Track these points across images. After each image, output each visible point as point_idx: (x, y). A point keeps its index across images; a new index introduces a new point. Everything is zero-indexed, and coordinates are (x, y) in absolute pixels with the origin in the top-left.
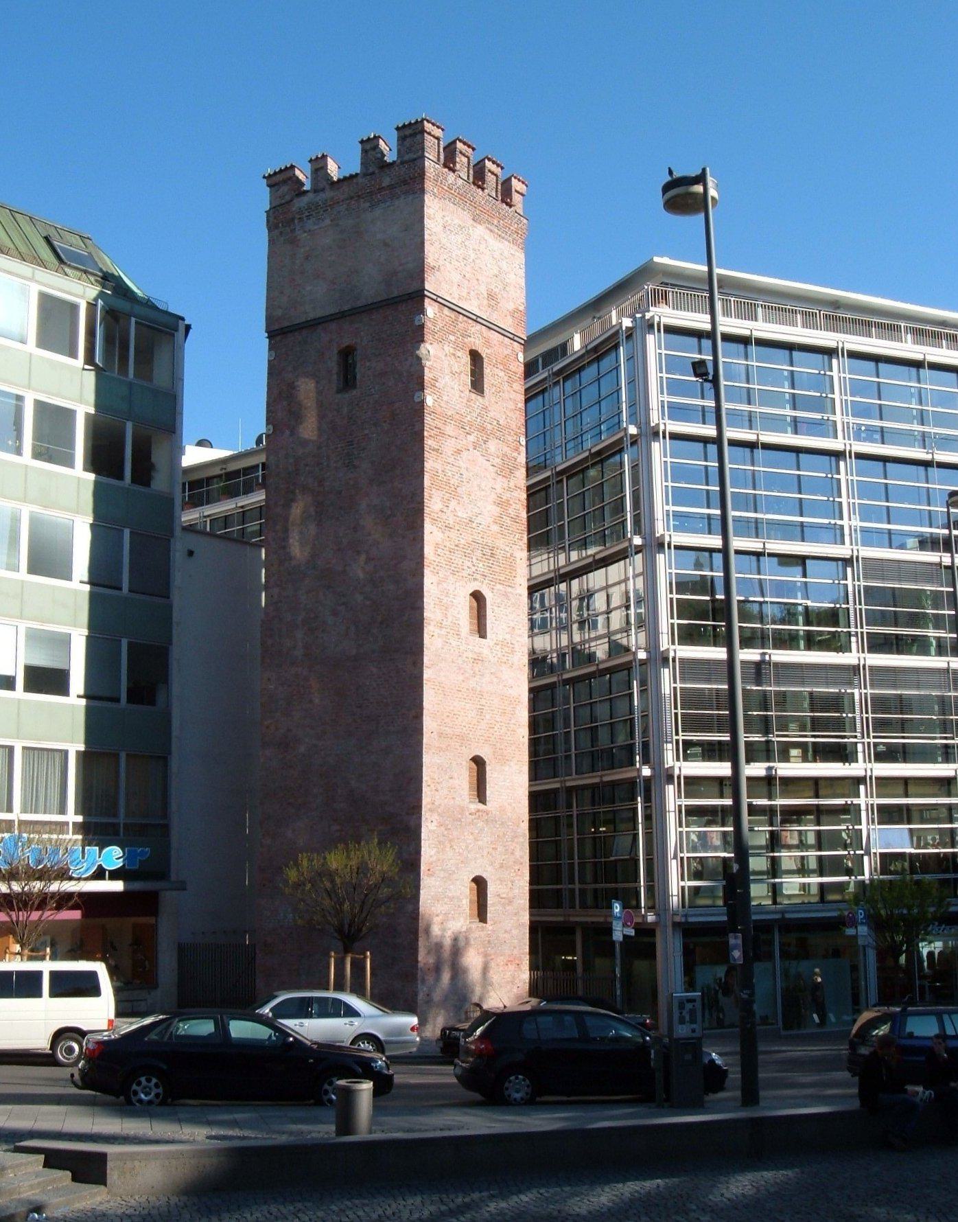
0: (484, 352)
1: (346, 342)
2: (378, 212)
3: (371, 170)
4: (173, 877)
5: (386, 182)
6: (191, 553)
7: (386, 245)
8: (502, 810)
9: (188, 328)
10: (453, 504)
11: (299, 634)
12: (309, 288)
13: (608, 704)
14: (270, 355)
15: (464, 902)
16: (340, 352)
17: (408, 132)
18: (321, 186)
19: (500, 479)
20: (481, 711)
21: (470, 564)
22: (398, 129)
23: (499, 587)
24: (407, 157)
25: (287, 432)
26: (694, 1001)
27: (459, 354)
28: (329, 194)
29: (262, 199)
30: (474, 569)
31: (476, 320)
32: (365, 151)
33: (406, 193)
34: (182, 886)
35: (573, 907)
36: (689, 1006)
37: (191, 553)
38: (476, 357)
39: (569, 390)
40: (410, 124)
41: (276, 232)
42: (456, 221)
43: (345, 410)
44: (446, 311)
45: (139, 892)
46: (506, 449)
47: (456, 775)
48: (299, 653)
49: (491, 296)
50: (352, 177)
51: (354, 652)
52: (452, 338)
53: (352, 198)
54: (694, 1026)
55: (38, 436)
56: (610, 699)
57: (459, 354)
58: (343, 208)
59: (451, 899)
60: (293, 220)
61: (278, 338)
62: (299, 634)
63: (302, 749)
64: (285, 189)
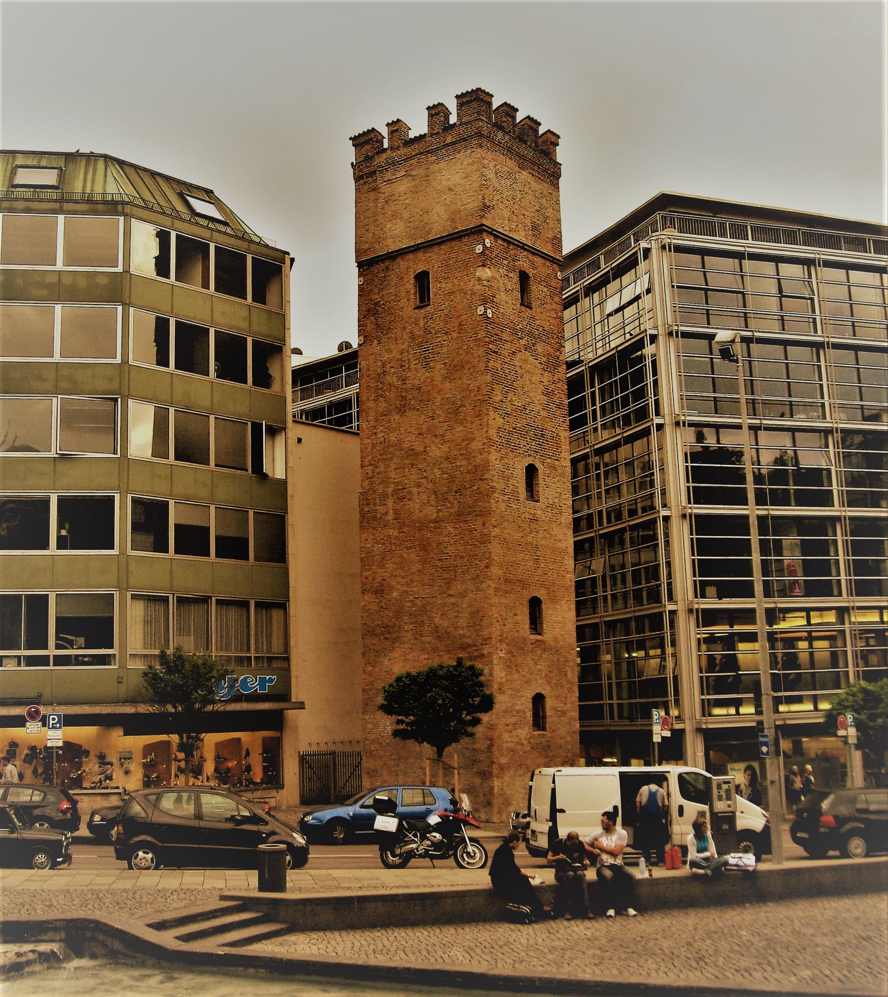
0: (531, 272)
2: (442, 165)
4: (293, 700)
5: (449, 140)
6: (300, 440)
7: (450, 189)
9: (292, 260)
11: (390, 502)
16: (415, 277)
23: (549, 460)
25: (376, 342)
29: (350, 154)
31: (523, 247)
32: (431, 116)
34: (301, 706)
36: (725, 787)
38: (524, 278)
43: (422, 323)
46: (550, 349)
47: (518, 612)
48: (390, 517)
49: (535, 227)
51: (435, 515)
59: (518, 712)
62: (390, 502)
63: (395, 594)
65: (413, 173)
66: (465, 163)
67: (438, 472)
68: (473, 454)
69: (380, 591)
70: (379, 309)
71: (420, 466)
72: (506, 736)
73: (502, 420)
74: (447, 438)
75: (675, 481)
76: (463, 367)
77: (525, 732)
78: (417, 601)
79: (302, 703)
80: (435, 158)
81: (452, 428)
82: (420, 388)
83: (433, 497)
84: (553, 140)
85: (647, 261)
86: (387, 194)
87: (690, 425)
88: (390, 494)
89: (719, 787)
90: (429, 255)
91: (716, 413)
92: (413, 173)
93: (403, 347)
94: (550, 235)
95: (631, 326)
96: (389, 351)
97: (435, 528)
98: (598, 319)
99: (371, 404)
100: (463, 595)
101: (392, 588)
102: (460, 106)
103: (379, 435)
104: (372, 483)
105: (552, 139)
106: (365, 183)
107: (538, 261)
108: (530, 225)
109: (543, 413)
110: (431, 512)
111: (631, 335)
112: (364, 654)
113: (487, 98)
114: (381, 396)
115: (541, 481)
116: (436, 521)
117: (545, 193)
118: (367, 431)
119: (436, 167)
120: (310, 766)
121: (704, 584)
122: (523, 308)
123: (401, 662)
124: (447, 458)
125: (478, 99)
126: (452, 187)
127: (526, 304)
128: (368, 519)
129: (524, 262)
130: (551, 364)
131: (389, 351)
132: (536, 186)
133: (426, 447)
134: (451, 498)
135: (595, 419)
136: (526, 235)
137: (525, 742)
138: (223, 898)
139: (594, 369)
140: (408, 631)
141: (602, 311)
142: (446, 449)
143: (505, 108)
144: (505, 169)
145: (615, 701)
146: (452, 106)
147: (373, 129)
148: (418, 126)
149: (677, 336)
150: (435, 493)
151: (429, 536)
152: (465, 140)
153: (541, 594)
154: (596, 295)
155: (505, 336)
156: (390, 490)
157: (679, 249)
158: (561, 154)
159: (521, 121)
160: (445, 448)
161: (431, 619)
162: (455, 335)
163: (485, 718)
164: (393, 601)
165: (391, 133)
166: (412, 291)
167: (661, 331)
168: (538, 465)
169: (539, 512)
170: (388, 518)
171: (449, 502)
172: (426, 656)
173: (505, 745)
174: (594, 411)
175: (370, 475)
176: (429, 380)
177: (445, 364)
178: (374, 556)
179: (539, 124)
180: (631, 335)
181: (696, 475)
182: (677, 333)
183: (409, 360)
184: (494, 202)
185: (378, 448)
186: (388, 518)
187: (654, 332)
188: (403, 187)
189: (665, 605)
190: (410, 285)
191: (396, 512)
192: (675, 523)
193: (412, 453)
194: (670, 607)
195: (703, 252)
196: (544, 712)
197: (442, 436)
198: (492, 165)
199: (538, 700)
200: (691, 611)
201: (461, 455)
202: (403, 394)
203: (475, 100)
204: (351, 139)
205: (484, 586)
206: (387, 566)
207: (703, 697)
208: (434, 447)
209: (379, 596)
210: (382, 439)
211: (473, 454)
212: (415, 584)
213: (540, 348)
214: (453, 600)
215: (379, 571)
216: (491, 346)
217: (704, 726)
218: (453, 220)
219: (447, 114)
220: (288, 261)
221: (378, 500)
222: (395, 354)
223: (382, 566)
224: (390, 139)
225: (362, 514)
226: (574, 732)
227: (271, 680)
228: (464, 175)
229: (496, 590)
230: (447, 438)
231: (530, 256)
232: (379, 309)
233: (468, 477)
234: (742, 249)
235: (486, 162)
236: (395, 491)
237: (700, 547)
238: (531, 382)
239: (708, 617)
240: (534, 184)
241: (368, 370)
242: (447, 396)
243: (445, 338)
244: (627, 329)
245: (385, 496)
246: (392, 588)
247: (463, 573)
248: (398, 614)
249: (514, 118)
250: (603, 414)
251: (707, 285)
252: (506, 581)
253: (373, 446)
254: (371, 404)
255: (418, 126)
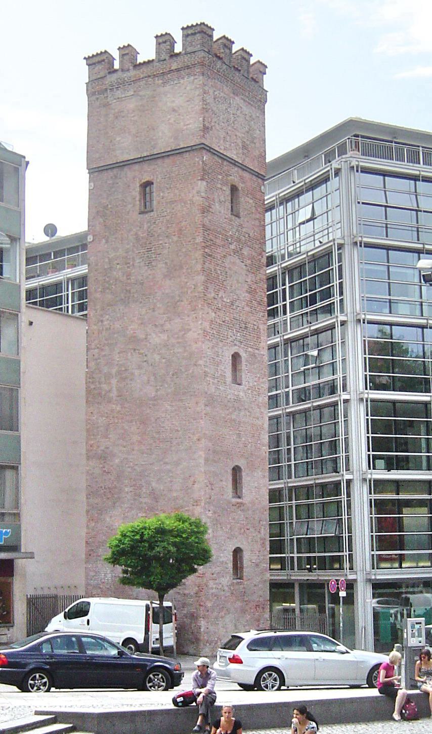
0: (240, 186)
1: (146, 178)
2: (168, 88)
3: (163, 57)
4: (23, 550)
5: (174, 66)
6: (31, 323)
7: (174, 110)
8: (253, 503)
9: (27, 163)
10: (221, 294)
11: (114, 381)
12: (118, 139)
13: (319, 427)
14: (90, 186)
15: (229, 565)
16: (141, 185)
17: (190, 32)
18: (126, 67)
19: (250, 275)
20: (239, 435)
21: (230, 334)
22: (183, 29)
23: (250, 349)
24: (189, 49)
25: (104, 241)
26: (420, 623)
27: (224, 188)
28: (132, 73)
29: (83, 73)
30: (234, 337)
31: (234, 163)
32: (158, 44)
33: (189, 75)
34: (31, 556)
35: (293, 569)
36: (417, 626)
37: (31, 323)
38: (234, 189)
39: (289, 211)
40: (192, 26)
41: (94, 98)
42: (222, 94)
43: (146, 226)
44: (216, 157)
45: (6, 560)
46: (254, 254)
47: (224, 479)
48: (114, 394)
49: (244, 147)
50: (149, 62)
51: (153, 394)
52: (220, 177)
53: (149, 76)
54: (420, 639)
55: (369, 370)
56: (321, 426)
57: (224, 188)
58: (142, 83)
59: (222, 563)
60: (106, 90)
61: (96, 174)
62: (114, 381)
63: (117, 461)
64: (100, 67)
65: (141, 93)
66: (188, 88)
67: (157, 357)
68: (189, 344)
69: (104, 457)
70: (107, 212)
71: (142, 351)
72: (211, 584)
73: (213, 314)
74: (166, 328)
75: (355, 371)
76: (181, 267)
77: (227, 580)
78: (136, 467)
79: (32, 553)
80: (161, 81)
81: (170, 319)
82: (142, 284)
83: (152, 378)
84: (261, 70)
85: (338, 178)
86: (116, 110)
87: (370, 322)
88: (114, 374)
89: (413, 627)
90: (153, 167)
91: (390, 313)
92: (141, 93)
93: (128, 247)
94: (257, 153)
95: (321, 234)
96: (116, 249)
97: (154, 405)
98: (290, 226)
99: (98, 295)
100: (177, 463)
101: (113, 455)
102: (185, 36)
103: (105, 323)
104: (97, 364)
105: (262, 68)
106: (97, 99)
107: (246, 175)
108: (240, 144)
109: (247, 309)
110: (150, 391)
111: (321, 242)
112: (88, 512)
113: (209, 32)
114: (108, 288)
115: (244, 367)
116: (155, 399)
117: (254, 116)
118: (94, 319)
119: (162, 89)
120: (36, 608)
121: (375, 457)
122: (233, 217)
123: (123, 522)
124: (166, 346)
125: (202, 32)
126: (176, 108)
127: (235, 212)
128: (94, 395)
129: (235, 175)
130: (254, 268)
131: (116, 249)
132: (246, 110)
133: (147, 335)
134: (169, 379)
135: (285, 313)
136: (237, 154)
137: (226, 588)
138: (38, 713)
139: (289, 271)
140: (127, 493)
141: (294, 220)
142: (166, 338)
143: (224, 41)
144: (222, 94)
145: (295, 555)
146: (178, 37)
147: (106, 52)
148: (147, 52)
149: (361, 246)
150: (154, 374)
151: (148, 411)
152: (188, 67)
153: (242, 463)
154: (289, 204)
155: (218, 241)
156: (114, 371)
157: (365, 171)
158: (268, 82)
159: (236, 53)
160: (164, 337)
161: (149, 483)
162: (175, 239)
163: (201, 569)
164: (115, 467)
165: (122, 56)
166: (137, 199)
167: (348, 241)
168: (243, 355)
169: (241, 394)
170: (111, 395)
171: (167, 383)
172: (144, 515)
173: (211, 591)
174: (285, 306)
175: (96, 356)
176: (151, 277)
177: (166, 263)
178: (98, 427)
179: (251, 55)
180: (321, 242)
181: (373, 365)
182: (361, 243)
183: (133, 258)
184: (213, 124)
185: (104, 333)
186: (111, 395)
187: (341, 242)
188: (132, 105)
189: (343, 475)
190: (136, 192)
191: (119, 390)
192: (353, 405)
193: (134, 339)
194: (348, 477)
195: (385, 174)
196: (242, 563)
197: (162, 325)
198: (211, 91)
199: (237, 552)
200: (365, 480)
201: (178, 343)
202: (128, 288)
203: (199, 32)
204: (85, 58)
205: (196, 456)
206: (110, 436)
207: (373, 553)
208: (154, 336)
209: (102, 462)
210: (108, 327)
211: (189, 344)
212: (134, 452)
213: (246, 251)
214: (168, 467)
215: (103, 440)
216: (206, 250)
217: (373, 577)
218: (176, 138)
219: (173, 43)
220: (24, 164)
221: (103, 379)
222: (121, 252)
223: (106, 437)
224: (121, 62)
225: (89, 391)
226: (265, 581)
227: (6, 533)
228: (187, 99)
229: (206, 460)
230: (166, 328)
231: (240, 171)
232: (107, 212)
233: (184, 363)
234: (418, 173)
235: (206, 88)
236: (119, 373)
237: (374, 426)
238: (238, 282)
239: (379, 486)
240: (244, 108)
241: (97, 265)
242: (167, 291)
243: (166, 240)
244: (317, 237)
245: (108, 376)
246: (113, 455)
247: (178, 444)
248: (119, 477)
249: (230, 49)
250: (292, 310)
251: (387, 203)
252: (214, 452)
253: (100, 332)
254: (98, 295)
255: (147, 52)
